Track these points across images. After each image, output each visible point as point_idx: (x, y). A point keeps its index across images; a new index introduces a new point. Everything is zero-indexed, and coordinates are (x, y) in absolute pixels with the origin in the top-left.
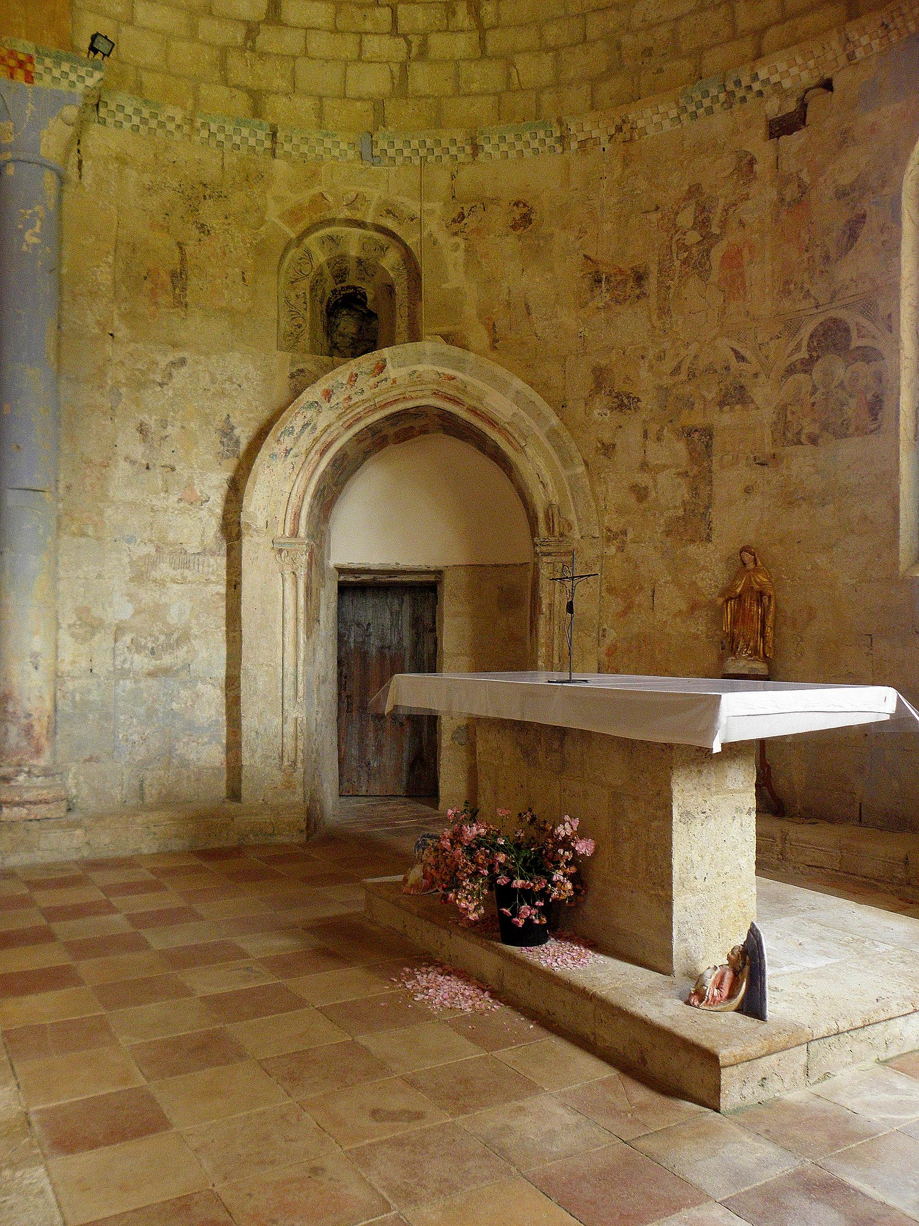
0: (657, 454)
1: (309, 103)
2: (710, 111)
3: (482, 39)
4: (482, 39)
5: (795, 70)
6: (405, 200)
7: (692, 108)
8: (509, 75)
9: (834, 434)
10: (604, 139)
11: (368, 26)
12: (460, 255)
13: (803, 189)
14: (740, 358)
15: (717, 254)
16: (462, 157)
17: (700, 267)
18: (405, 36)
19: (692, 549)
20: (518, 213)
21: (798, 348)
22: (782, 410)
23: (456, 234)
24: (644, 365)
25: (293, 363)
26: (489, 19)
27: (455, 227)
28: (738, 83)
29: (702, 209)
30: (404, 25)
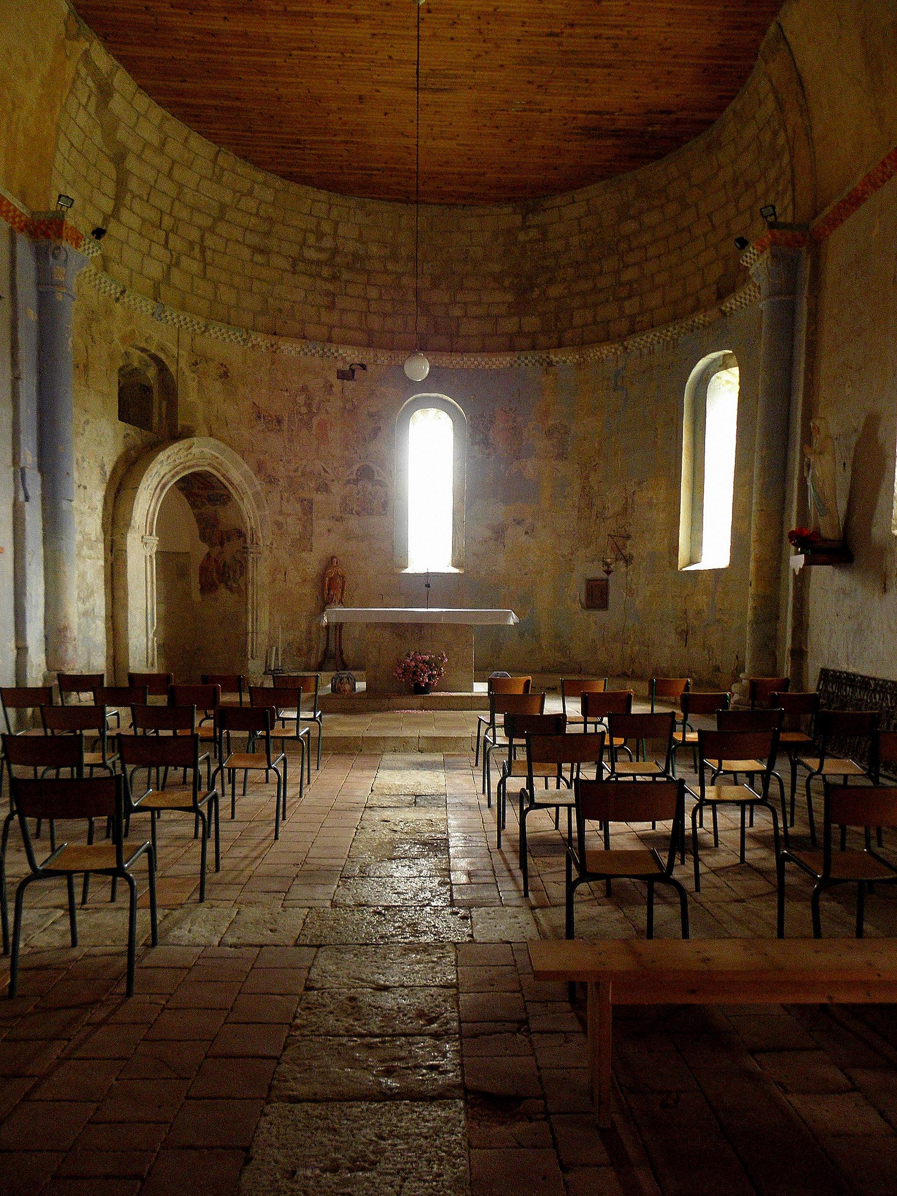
0: (287, 508)
1: (127, 271)
3: (205, 268)
4: (205, 268)
5: (353, 356)
6: (170, 345)
8: (216, 294)
9: (367, 512)
10: (264, 347)
12: (195, 383)
13: (355, 407)
15: (315, 421)
17: (307, 425)
20: (223, 369)
21: (352, 473)
22: (344, 499)
23: (194, 372)
24: (281, 463)
25: (125, 430)
26: (209, 260)
28: (329, 350)
30: (171, 245)
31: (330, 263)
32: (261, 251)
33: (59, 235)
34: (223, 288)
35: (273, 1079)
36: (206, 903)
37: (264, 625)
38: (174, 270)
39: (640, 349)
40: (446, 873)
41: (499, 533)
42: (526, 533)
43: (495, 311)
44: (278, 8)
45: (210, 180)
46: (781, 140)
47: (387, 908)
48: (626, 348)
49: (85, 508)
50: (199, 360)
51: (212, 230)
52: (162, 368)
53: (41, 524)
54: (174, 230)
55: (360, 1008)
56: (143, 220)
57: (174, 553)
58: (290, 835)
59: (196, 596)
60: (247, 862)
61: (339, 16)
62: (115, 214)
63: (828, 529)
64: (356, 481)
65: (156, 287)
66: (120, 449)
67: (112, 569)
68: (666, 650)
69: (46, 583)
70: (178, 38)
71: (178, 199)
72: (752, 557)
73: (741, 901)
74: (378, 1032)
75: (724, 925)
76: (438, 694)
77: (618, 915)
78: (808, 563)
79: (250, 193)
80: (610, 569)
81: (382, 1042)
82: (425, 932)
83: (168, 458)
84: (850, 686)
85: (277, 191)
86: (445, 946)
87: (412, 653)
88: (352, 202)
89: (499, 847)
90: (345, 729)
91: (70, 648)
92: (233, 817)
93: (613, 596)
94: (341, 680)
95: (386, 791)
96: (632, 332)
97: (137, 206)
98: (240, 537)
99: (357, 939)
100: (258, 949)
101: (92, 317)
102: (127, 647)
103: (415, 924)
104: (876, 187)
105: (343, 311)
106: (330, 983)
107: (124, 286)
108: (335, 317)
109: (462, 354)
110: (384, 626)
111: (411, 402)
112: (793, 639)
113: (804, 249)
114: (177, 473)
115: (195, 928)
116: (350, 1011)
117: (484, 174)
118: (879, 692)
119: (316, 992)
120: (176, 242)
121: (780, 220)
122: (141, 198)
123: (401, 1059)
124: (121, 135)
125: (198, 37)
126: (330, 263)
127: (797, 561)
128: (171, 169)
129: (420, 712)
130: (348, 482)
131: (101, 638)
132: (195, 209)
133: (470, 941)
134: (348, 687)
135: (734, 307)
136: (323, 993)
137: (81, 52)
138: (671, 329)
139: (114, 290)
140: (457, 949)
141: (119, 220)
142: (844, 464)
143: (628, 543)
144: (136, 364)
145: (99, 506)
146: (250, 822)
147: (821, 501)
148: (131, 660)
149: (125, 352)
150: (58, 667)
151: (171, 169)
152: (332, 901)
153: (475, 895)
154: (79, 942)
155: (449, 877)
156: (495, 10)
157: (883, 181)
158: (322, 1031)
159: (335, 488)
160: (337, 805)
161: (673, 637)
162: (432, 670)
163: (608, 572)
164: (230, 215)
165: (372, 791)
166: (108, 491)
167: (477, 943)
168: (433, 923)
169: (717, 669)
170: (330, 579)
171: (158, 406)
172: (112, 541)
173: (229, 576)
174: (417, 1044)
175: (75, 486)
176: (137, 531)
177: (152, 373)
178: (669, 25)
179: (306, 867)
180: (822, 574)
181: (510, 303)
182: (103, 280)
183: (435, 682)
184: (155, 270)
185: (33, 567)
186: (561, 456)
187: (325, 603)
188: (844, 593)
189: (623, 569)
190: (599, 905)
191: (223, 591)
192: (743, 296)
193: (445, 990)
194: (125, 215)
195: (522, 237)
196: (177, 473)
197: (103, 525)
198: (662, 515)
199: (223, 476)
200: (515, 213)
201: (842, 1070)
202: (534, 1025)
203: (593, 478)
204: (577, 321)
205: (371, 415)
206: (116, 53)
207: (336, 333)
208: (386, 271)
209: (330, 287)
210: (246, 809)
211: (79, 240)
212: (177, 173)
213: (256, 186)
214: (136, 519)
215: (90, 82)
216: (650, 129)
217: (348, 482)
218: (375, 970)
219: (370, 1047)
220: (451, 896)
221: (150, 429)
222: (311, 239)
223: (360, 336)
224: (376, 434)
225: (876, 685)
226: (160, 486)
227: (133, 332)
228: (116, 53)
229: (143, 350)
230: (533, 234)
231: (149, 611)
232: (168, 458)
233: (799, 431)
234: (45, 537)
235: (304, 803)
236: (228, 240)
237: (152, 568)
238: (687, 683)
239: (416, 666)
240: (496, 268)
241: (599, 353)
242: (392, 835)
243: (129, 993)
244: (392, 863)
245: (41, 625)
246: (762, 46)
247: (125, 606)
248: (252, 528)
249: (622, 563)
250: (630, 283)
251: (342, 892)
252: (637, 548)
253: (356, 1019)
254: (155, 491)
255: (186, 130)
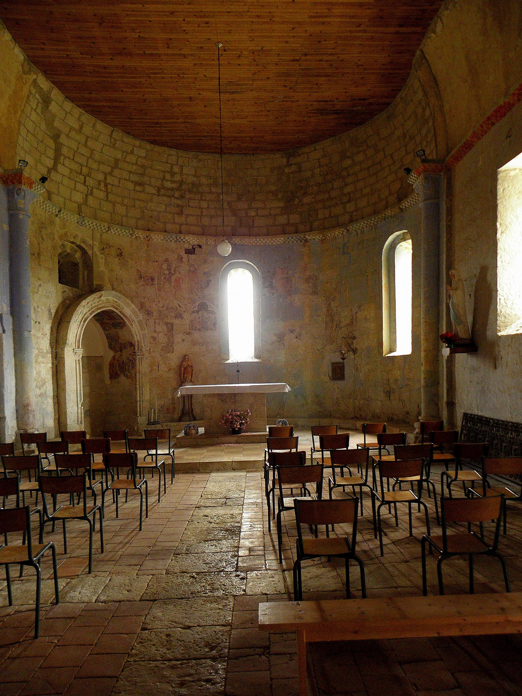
0: (159, 328)
2: (171, 241)
3: (107, 195)
4: (107, 195)
5: (194, 240)
7: (167, 239)
8: (114, 209)
10: (142, 238)
11: (78, 180)
14: (180, 306)
15: (173, 278)
16: (104, 231)
18: (87, 186)
19: (168, 354)
20: (119, 252)
22: (191, 321)
23: (102, 254)
26: (109, 190)
27: (102, 251)
28: (180, 238)
29: (169, 265)
31: (178, 189)
32: (140, 184)
33: (20, 182)
34: (118, 206)
35: (112, 692)
36: (93, 574)
37: (147, 396)
38: (90, 197)
39: (356, 231)
40: (236, 549)
41: (281, 338)
42: (296, 337)
43: (273, 212)
44: (141, 52)
45: (109, 146)
46: (428, 113)
47: (198, 574)
48: (348, 231)
49: (39, 334)
50: (105, 247)
51: (111, 173)
52: (84, 252)
53: (12, 346)
54: (89, 175)
55: (171, 641)
56: (71, 170)
57: (94, 357)
58: (149, 527)
59: (107, 381)
60: (121, 546)
61: (174, 55)
62: (55, 168)
63: (462, 332)
64: (198, 312)
65: (80, 207)
66: (60, 299)
67: (56, 369)
68: (379, 403)
69: (16, 379)
70: (85, 70)
71: (90, 157)
72: (422, 349)
73: (407, 561)
74: (180, 657)
75: (395, 578)
76: (246, 434)
77: (334, 573)
78: (452, 352)
79: (132, 152)
80: (344, 357)
81: (181, 664)
82: (218, 589)
83: (88, 304)
84: (480, 423)
85: (147, 151)
86: (228, 598)
87: (230, 411)
88: (191, 154)
89: (270, 531)
90: (190, 458)
91: (31, 416)
92: (117, 517)
93: (347, 371)
94: (190, 428)
95: (209, 496)
96: (351, 221)
97: (67, 162)
98: (131, 346)
99: (177, 595)
100: (118, 603)
101: (42, 226)
102: (66, 413)
103: (213, 584)
104: (479, 139)
105: (187, 215)
106: (157, 624)
107: (60, 208)
108: (182, 219)
109: (256, 236)
110: (214, 395)
111: (228, 265)
112: (447, 395)
113: (442, 173)
114: (93, 312)
115: (83, 591)
116: (165, 643)
117: (264, 136)
118: (495, 427)
119: (147, 631)
120: (90, 182)
121: (430, 158)
122: (69, 158)
123: (190, 675)
124: (56, 124)
125: (96, 69)
126: (178, 189)
127: (446, 351)
128: (86, 141)
129: (235, 445)
130: (193, 312)
131: (51, 408)
132: (100, 163)
133: (243, 594)
134: (193, 432)
135: (407, 206)
136: (151, 632)
137: (32, 80)
138: (373, 219)
139: (55, 210)
140: (235, 599)
141: (57, 171)
142: (470, 295)
143: (355, 341)
144: (68, 251)
145: (48, 333)
146: (127, 519)
147: (457, 317)
148: (69, 422)
149: (62, 245)
150: (23, 427)
151: (86, 141)
152: (166, 570)
153: (251, 563)
154: (14, 602)
155: (238, 552)
156: (262, 48)
157: (483, 136)
158: (147, 657)
159: (186, 316)
160: (180, 507)
161: (382, 394)
162: (242, 421)
163: (343, 359)
164: (121, 165)
165: (201, 496)
166: (53, 323)
167: (247, 595)
168: (223, 583)
169: (407, 413)
170: (185, 368)
171: (82, 274)
172: (56, 352)
173: (126, 369)
174: (201, 665)
175: (33, 322)
176: (71, 346)
177: (78, 255)
178: (360, 53)
179: (156, 548)
180: (461, 358)
181: (282, 208)
182: (48, 205)
183: (244, 427)
184: (78, 197)
185: (8, 371)
186: (315, 293)
187: (182, 383)
188: (474, 369)
189: (352, 357)
190: (323, 567)
191: (122, 378)
192: (412, 199)
193: (223, 628)
194: (60, 168)
195: (287, 170)
196: (93, 312)
197: (50, 343)
198: (373, 325)
199: (120, 312)
200: (282, 157)
201: (453, 674)
202: (274, 649)
203: (333, 304)
204: (320, 216)
205: (205, 273)
206: (52, 80)
207: (184, 228)
208: (211, 193)
209: (179, 202)
210: (126, 511)
211: (32, 185)
212: (89, 143)
213: (135, 148)
214: (69, 339)
215: (37, 96)
216: (355, 108)
217: (193, 312)
218: (184, 615)
219: (173, 667)
220: (237, 564)
221: (78, 288)
222: (168, 176)
223: (198, 229)
224: (208, 284)
225: (494, 422)
226: (83, 320)
227: (66, 234)
228: (52, 80)
229: (72, 243)
230: (294, 168)
231: (79, 391)
232: (88, 304)
233: (445, 276)
234: (15, 353)
235: (160, 506)
236: (120, 179)
237: (80, 366)
238: (385, 426)
239: (232, 418)
240: (273, 188)
241: (333, 234)
242: (208, 525)
243: (36, 637)
244: (205, 543)
245: (13, 404)
246: (414, 62)
247: (64, 390)
248: (138, 341)
249: (351, 353)
250: (349, 193)
251: (173, 564)
252: (360, 344)
253: (168, 649)
254: (80, 323)
255: (94, 119)
